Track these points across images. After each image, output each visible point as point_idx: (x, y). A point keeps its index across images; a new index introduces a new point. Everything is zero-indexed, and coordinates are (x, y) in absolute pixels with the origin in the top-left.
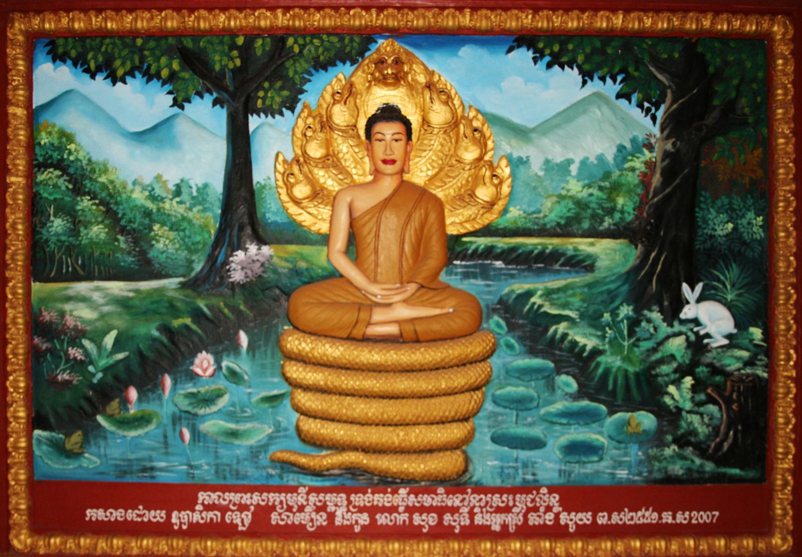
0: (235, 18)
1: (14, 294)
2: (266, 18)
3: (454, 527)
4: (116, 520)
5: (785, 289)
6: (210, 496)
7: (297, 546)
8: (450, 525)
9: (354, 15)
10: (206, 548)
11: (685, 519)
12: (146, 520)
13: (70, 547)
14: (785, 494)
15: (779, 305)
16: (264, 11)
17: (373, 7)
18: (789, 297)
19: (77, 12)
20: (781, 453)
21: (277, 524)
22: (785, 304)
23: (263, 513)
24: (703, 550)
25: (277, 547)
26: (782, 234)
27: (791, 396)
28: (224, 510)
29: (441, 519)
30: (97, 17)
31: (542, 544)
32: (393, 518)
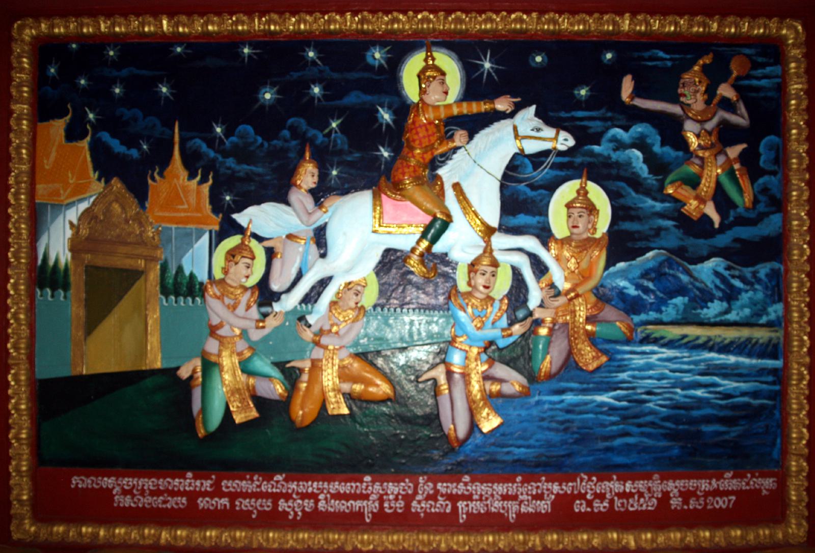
3: (288, 513)
4: (144, 506)
6: (83, 481)
8: (284, 511)
10: (268, 539)
11: (700, 505)
12: (169, 506)
13: (135, 538)
20: (796, 438)
22: (19, 338)
23: (563, 503)
24: (690, 542)
26: (23, 407)
27: (805, 382)
28: (314, 496)
29: (275, 504)
31: (610, 535)
32: (214, 502)
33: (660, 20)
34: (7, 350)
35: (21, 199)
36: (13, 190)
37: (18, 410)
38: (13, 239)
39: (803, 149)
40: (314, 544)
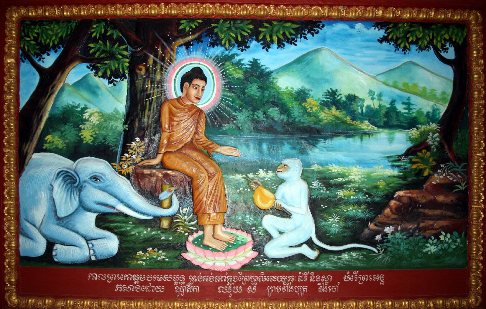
0: (192, 8)
1: (9, 161)
2: (210, 8)
5: (478, 159)
7: (172, 304)
9: (260, 9)
14: (477, 274)
15: (473, 168)
16: (209, 4)
17: (181, 3)
18: (480, 164)
19: (100, 5)
21: (251, 292)
22: (478, 168)
25: (161, 305)
26: (476, 128)
30: (111, 8)
33: (401, 11)
34: (4, 195)
35: (11, 109)
36: (480, 253)
37: (9, 230)
38: (7, 132)
39: (480, 45)
40: (292, 9)
